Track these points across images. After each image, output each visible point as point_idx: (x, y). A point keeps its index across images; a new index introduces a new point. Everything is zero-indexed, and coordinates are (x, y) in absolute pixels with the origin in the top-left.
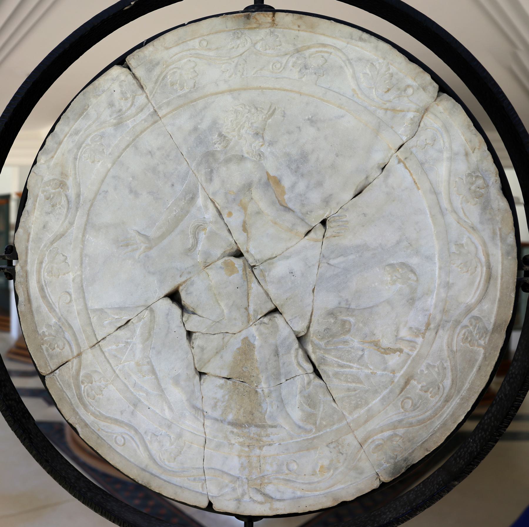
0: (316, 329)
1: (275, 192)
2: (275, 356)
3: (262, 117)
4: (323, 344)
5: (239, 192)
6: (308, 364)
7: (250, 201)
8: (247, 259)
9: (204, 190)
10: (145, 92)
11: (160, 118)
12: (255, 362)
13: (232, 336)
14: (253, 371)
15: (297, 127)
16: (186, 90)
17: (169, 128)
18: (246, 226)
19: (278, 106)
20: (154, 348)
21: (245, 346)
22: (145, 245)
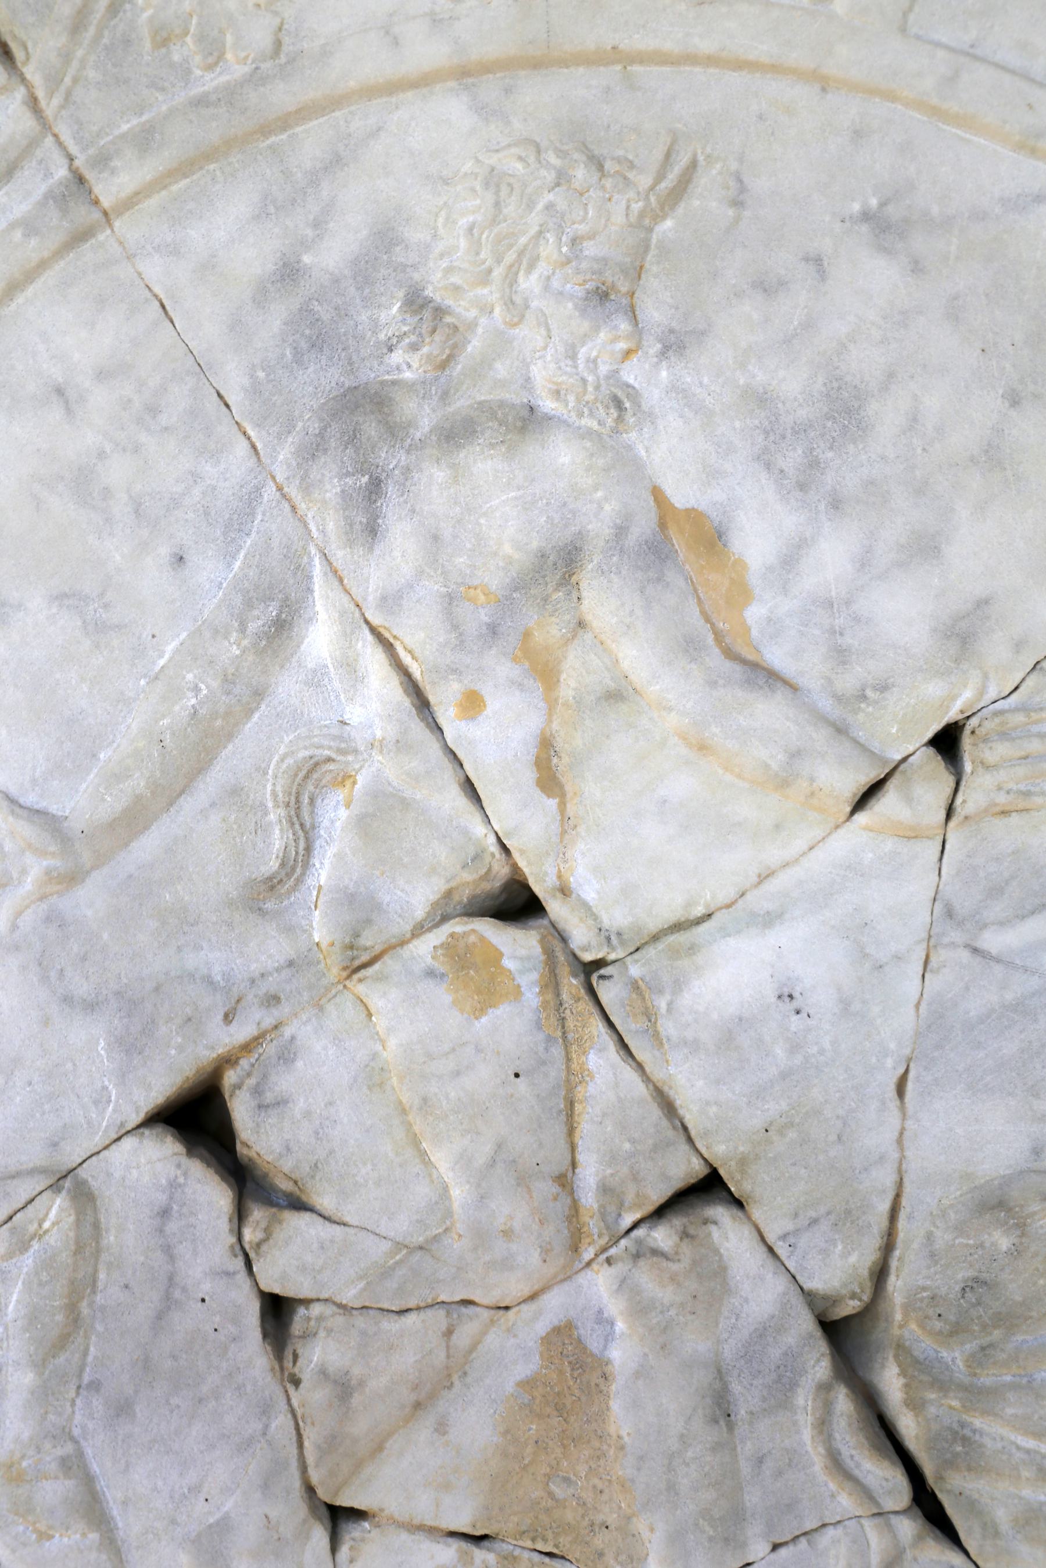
0: (920, 1283)
1: (696, 591)
2: (717, 1422)
3: (628, 207)
4: (960, 1363)
5: (516, 589)
6: (886, 1464)
7: (574, 637)
8: (561, 926)
9: (341, 580)
10: (23, 79)
11: (105, 213)
12: (612, 1452)
13: (492, 1321)
14: (605, 1497)
15: (807, 259)
16: (235, 69)
17: (153, 269)
18: (555, 760)
19: (708, 150)
20: (95, 1386)
21: (561, 1372)
22: (45, 863)
